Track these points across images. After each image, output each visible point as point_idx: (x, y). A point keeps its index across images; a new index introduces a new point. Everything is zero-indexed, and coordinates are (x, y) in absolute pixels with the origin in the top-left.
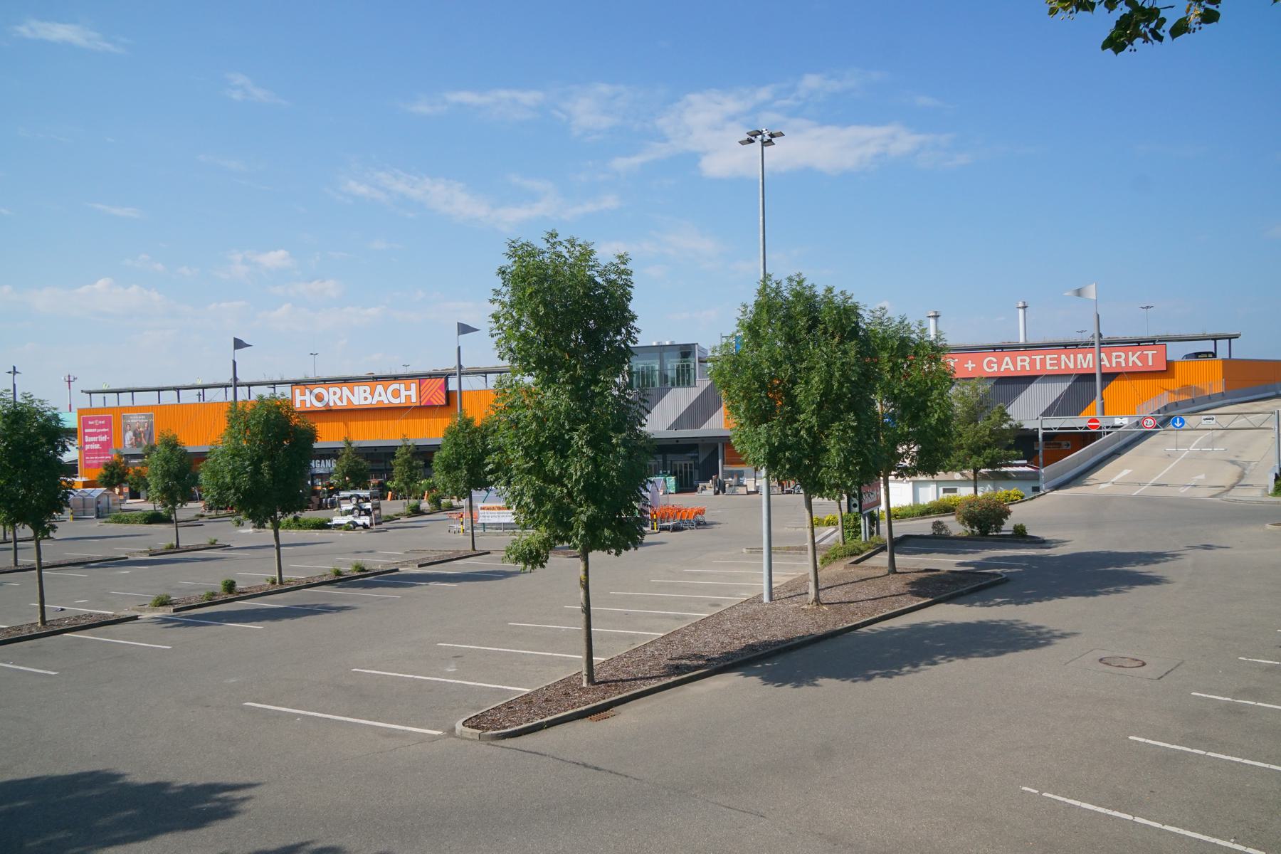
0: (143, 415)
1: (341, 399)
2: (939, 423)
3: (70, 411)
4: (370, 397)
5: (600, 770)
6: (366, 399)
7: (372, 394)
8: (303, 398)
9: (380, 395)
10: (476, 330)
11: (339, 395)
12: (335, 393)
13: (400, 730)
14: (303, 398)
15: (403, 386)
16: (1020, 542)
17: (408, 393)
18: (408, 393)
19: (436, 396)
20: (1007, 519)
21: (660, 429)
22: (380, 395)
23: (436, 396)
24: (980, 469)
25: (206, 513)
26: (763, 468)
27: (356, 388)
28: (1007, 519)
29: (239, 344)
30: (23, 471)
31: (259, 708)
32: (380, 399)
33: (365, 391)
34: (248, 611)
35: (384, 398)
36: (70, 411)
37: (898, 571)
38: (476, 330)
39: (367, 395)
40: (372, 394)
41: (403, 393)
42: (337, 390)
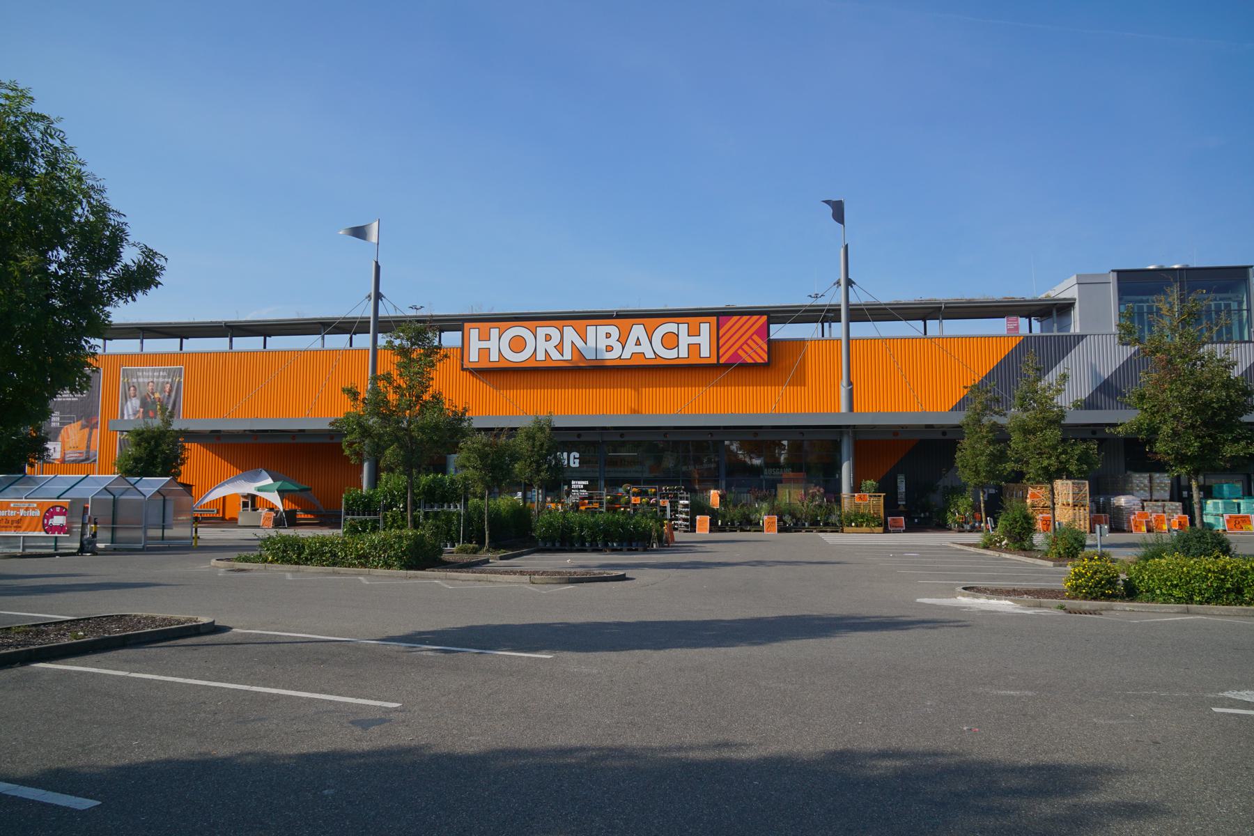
1: (560, 347)
4: (618, 346)
7: (623, 341)
8: (484, 345)
9: (638, 343)
10: (823, 201)
12: (548, 338)
22: (638, 343)
32: (638, 349)
33: (608, 336)
35: (645, 349)
38: (823, 201)
39: (612, 342)
40: (623, 341)
41: (685, 340)
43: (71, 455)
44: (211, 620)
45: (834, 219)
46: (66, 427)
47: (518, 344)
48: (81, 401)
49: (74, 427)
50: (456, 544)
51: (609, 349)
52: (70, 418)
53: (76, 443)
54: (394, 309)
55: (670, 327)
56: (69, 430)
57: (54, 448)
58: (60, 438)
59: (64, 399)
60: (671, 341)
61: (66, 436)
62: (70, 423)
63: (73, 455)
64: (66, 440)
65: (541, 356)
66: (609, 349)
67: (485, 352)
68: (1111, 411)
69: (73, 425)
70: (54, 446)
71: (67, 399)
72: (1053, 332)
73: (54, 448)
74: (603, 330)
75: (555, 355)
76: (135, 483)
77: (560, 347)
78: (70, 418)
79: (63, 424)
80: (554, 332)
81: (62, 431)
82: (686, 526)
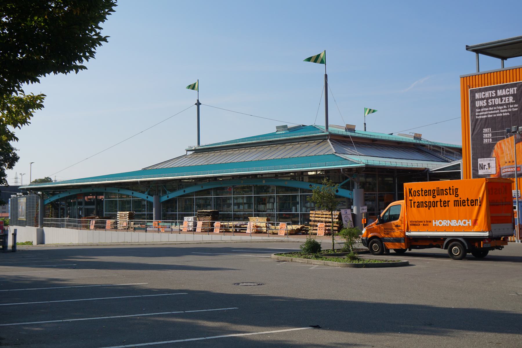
0: (114, 226)
1: (447, 224)
4: (456, 223)
6: (455, 224)
8: (435, 223)
10: (107, 20)
12: (445, 222)
13: (276, 333)
14: (435, 223)
15: (467, 220)
20: (32, 83)
21: (24, 184)
22: (460, 223)
24: (85, 200)
27: (452, 221)
28: (32, 83)
29: (19, 150)
31: (175, 343)
32: (460, 224)
33: (455, 222)
35: (461, 224)
37: (516, 145)
38: (107, 20)
39: (456, 223)
41: (467, 223)
42: (446, 221)
43: (506, 170)
44: (407, 261)
46: (498, 142)
48: (514, 115)
49: (508, 142)
50: (81, 208)
52: (502, 134)
53: (511, 157)
56: (503, 145)
57: (489, 164)
58: (494, 154)
59: (495, 115)
61: (499, 152)
62: (504, 138)
63: (509, 170)
64: (500, 155)
66: (455, 224)
69: (505, 139)
70: (489, 162)
71: (498, 115)
73: (489, 164)
75: (447, 225)
78: (502, 134)
79: (495, 140)
81: (496, 147)
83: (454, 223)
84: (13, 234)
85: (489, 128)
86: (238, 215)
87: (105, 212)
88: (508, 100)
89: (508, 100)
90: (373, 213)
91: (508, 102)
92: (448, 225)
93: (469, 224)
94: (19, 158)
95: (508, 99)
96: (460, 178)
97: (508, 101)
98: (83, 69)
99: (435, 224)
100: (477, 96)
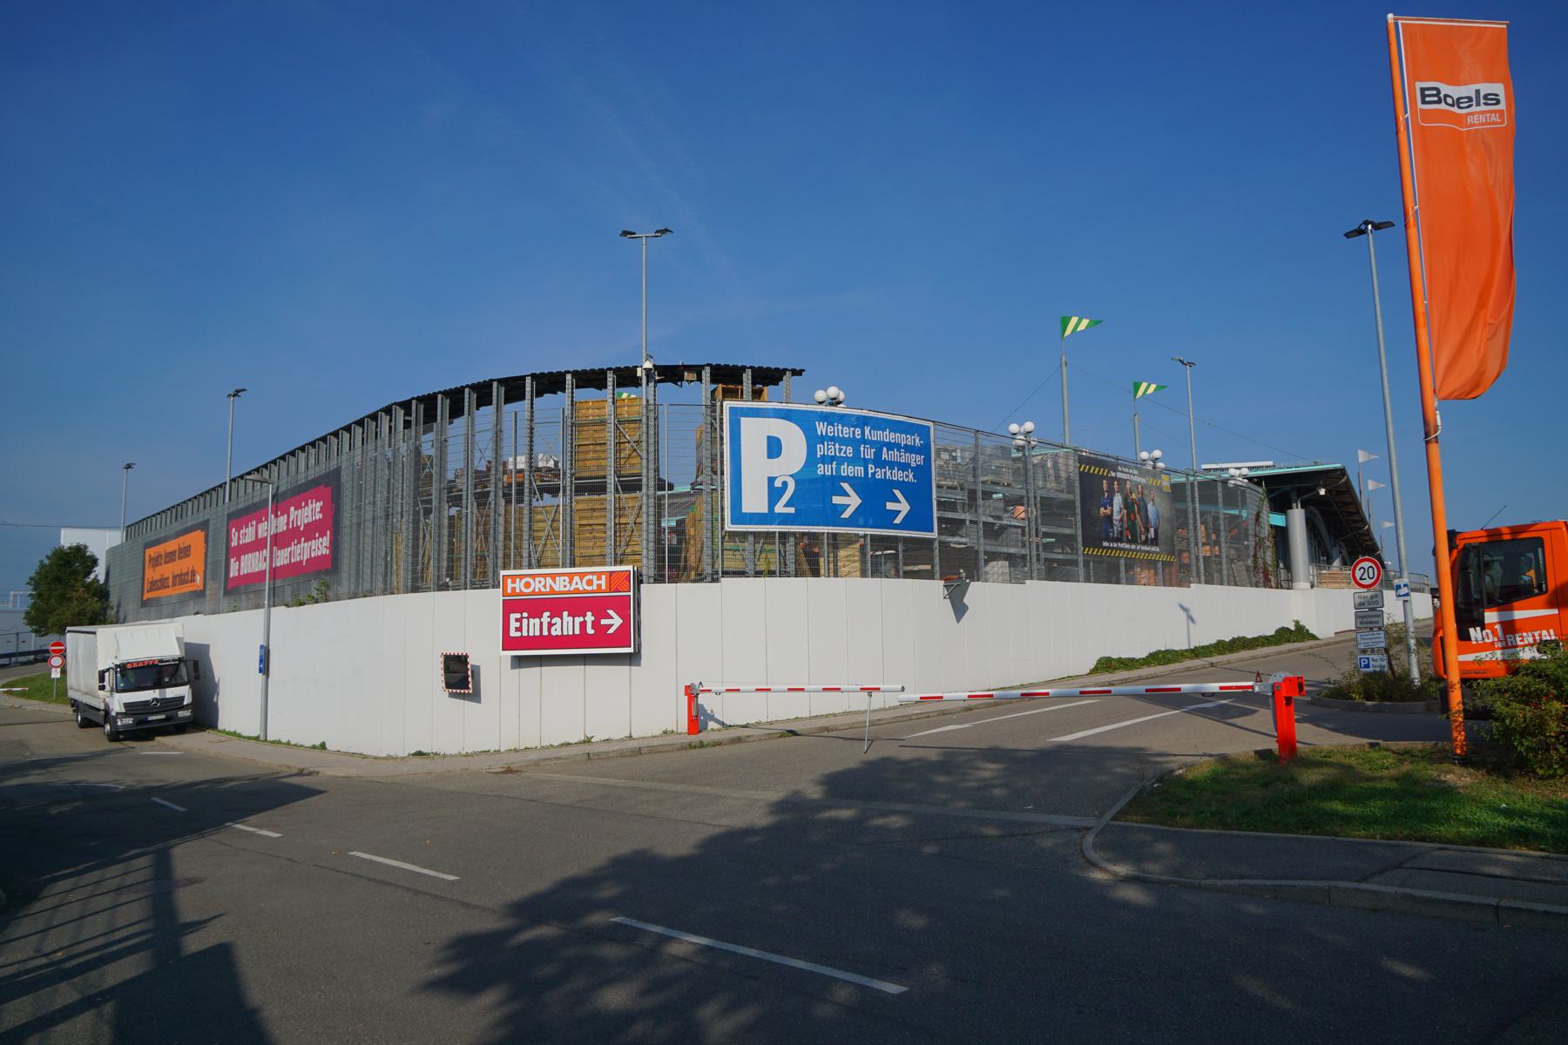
1: (545, 586)
2: (52, 620)
3: (516, 413)
4: (568, 585)
5: (799, 735)
6: (565, 586)
7: (571, 583)
8: (513, 585)
9: (577, 584)
10: (325, 792)
11: (543, 583)
12: (540, 582)
16: (1442, 615)
17: (599, 582)
18: (599, 582)
19: (910, 449)
22: (577, 584)
23: (910, 449)
25: (1358, 698)
26: (489, 998)
30: (1561, 832)
34: (131, 939)
36: (516, 413)
38: (325, 792)
39: (567, 583)
40: (571, 583)
41: (596, 583)
45: (778, 438)
47: (527, 585)
51: (565, 586)
54: (728, 723)
55: (590, 577)
60: (590, 583)
65: (537, 590)
67: (514, 589)
68: (832, 579)
72: (938, 510)
74: (562, 578)
76: (73, 720)
77: (545, 586)
80: (542, 580)
82: (312, 503)
83: (562, 584)
84: (701, 742)
85: (528, 635)
86: (716, 443)
87: (905, 564)
88: (518, 624)
89: (518, 624)
90: (1185, 497)
91: (518, 634)
92: (548, 589)
93: (599, 586)
94: (1297, 622)
95: (517, 620)
96: (503, 650)
97: (1521, 641)
98: (1293, 628)
99: (514, 589)
100: (513, 633)
